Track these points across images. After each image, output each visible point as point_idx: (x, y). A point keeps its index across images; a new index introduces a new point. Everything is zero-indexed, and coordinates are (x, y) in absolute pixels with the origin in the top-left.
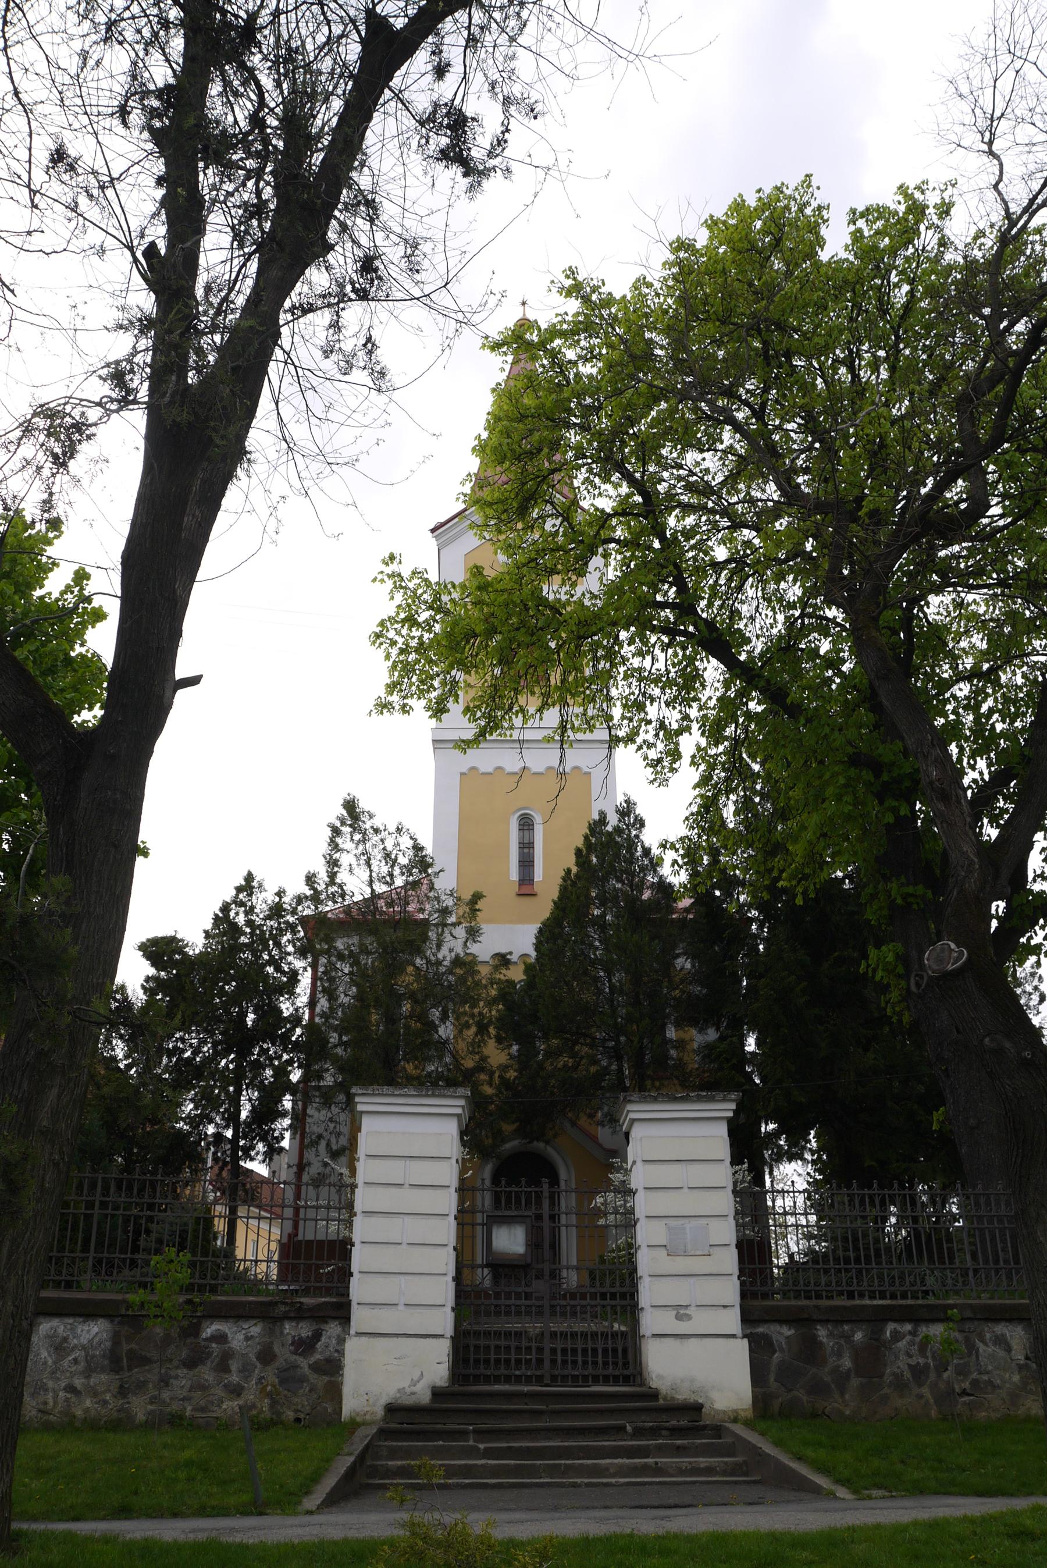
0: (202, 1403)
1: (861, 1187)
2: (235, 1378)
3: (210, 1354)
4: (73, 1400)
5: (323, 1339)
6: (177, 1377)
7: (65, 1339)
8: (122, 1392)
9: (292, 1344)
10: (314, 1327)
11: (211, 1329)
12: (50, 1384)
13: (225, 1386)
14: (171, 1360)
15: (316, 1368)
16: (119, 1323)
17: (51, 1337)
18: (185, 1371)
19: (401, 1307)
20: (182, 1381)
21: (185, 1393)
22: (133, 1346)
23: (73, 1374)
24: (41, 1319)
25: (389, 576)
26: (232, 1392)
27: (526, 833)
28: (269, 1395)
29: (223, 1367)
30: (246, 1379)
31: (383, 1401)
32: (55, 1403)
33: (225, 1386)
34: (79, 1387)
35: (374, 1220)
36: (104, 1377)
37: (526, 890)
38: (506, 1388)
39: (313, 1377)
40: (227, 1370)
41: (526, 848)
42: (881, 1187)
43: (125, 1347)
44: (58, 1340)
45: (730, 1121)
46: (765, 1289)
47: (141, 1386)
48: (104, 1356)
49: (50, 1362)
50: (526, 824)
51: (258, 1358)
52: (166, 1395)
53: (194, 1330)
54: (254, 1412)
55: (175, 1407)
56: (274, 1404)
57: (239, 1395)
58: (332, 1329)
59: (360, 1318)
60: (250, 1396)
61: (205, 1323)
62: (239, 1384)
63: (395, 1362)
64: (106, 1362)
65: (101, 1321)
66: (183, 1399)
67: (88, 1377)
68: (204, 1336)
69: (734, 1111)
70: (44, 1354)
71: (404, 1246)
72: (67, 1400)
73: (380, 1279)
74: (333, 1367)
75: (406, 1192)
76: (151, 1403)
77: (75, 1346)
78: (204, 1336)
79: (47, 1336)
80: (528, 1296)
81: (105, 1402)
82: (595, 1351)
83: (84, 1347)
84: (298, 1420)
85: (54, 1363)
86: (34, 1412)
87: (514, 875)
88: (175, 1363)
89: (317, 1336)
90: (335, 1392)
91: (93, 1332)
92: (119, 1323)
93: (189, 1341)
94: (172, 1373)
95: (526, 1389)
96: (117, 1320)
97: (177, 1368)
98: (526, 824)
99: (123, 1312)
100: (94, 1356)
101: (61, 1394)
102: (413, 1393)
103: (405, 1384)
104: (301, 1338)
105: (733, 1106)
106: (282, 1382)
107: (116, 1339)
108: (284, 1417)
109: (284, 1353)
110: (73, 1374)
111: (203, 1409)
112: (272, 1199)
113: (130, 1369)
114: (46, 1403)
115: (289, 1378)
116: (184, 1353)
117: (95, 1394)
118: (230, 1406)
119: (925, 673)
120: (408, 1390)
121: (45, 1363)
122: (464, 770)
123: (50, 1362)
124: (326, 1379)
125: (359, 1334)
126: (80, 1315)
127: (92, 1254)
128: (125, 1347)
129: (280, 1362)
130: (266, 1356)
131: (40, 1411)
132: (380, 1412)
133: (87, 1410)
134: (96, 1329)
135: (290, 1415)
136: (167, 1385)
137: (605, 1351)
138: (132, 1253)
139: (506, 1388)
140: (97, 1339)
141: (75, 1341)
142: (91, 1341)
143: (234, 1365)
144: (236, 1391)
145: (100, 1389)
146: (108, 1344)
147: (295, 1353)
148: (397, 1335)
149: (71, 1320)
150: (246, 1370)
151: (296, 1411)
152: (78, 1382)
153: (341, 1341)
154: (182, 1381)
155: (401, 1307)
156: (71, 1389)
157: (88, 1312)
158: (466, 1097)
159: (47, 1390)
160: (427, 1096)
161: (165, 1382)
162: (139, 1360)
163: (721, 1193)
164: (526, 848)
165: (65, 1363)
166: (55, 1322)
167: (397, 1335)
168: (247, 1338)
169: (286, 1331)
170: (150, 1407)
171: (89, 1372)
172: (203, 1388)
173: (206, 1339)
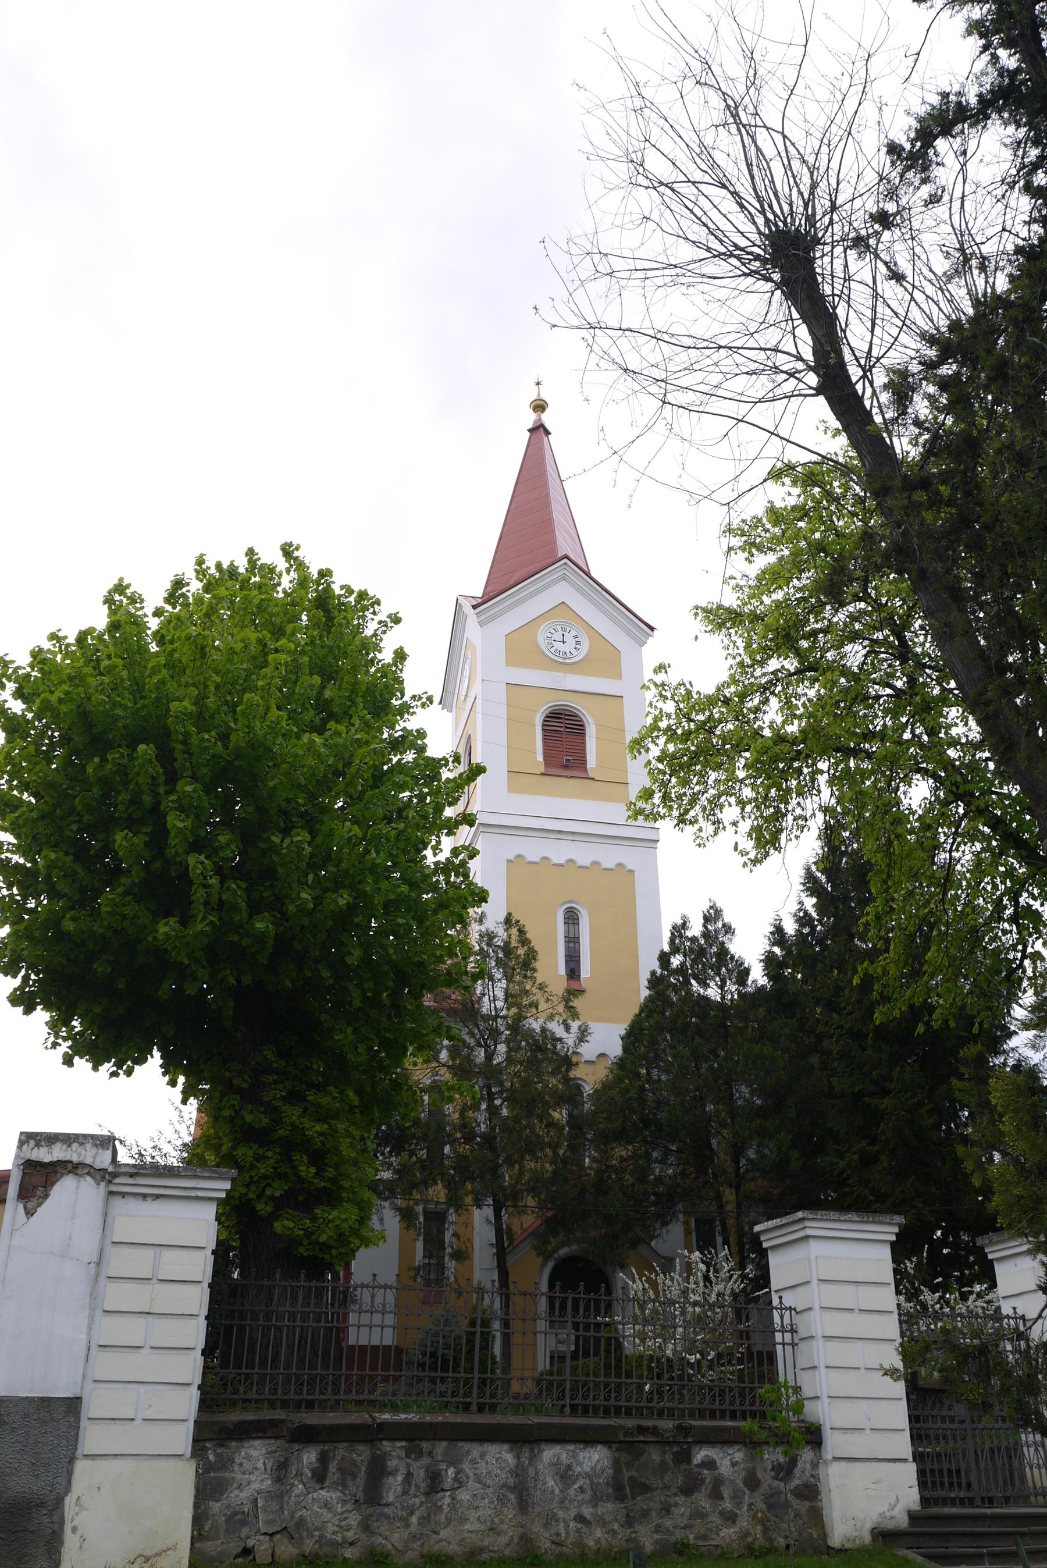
0: (703, 1531)
1: (588, 1291)
2: (727, 1505)
3: (703, 1480)
4: (584, 1529)
6: (676, 1505)
7: (569, 1467)
8: (629, 1522)
9: (773, 1469)
11: (701, 1454)
12: (561, 1514)
13: (720, 1513)
14: (669, 1488)
15: (798, 1493)
16: (617, 1450)
17: (556, 1464)
18: (683, 1498)
19: (868, 1432)
20: (682, 1508)
21: (685, 1521)
22: (633, 1473)
23: (581, 1503)
24: (543, 1446)
25: (656, 684)
26: (727, 1519)
27: (571, 927)
28: (761, 1521)
29: (716, 1495)
30: (739, 1505)
31: (868, 1526)
32: (567, 1533)
33: (720, 1513)
34: (588, 1517)
35: (834, 1345)
36: (610, 1506)
38: (954, 1510)
39: (795, 1503)
40: (719, 1497)
41: (572, 942)
42: (588, 1291)
43: (627, 1474)
44: (563, 1468)
46: (494, 1401)
47: (645, 1514)
48: (608, 1484)
49: (557, 1491)
50: (572, 918)
51: (745, 1484)
52: (668, 1523)
53: (685, 1457)
54: (750, 1540)
55: (678, 1535)
56: (766, 1531)
57: (734, 1522)
59: (834, 1443)
60: (744, 1522)
61: (695, 1449)
62: (732, 1511)
63: (873, 1486)
64: (610, 1490)
65: (599, 1447)
66: (684, 1528)
67: (595, 1506)
70: (551, 1483)
71: (862, 1371)
72: (578, 1531)
73: (847, 1404)
74: (811, 1492)
75: (857, 1317)
76: (657, 1532)
77: (579, 1474)
79: (551, 1464)
80: (952, 1420)
81: (615, 1532)
82: (941, 1471)
83: (588, 1476)
84: (788, 1547)
85: (562, 1491)
86: (548, 1544)
87: (562, 970)
88: (674, 1490)
89: (793, 1461)
90: (817, 1517)
91: (594, 1458)
92: (617, 1450)
94: (672, 1501)
95: (989, 1511)
96: (614, 1446)
97: (675, 1495)
98: (572, 918)
99: (622, 1438)
100: (598, 1484)
101: (572, 1524)
102: (892, 1518)
103: (884, 1508)
104: (779, 1464)
106: (770, 1507)
107: (616, 1464)
108: (775, 1544)
109: (766, 1478)
110: (581, 1503)
111: (704, 1538)
112: (372, 1305)
113: (634, 1497)
114: (558, 1534)
115: (775, 1504)
116: (680, 1481)
117: (604, 1524)
118: (728, 1534)
120: (888, 1515)
121: (553, 1492)
122: (511, 858)
123: (557, 1491)
124: (807, 1504)
125: (835, 1459)
126: (580, 1442)
127: (476, 1375)
128: (627, 1474)
129: (764, 1488)
130: (752, 1482)
131: (553, 1542)
132: (867, 1538)
133: (598, 1541)
134: (596, 1457)
135: (781, 1542)
136: (668, 1512)
137: (950, 1471)
138: (606, 1376)
139: (954, 1510)
140: (599, 1467)
141: (579, 1469)
142: (593, 1469)
143: (726, 1492)
144: (731, 1518)
145: (608, 1518)
146: (610, 1471)
147: (776, 1478)
148: (868, 1460)
149: (572, 1447)
150: (737, 1497)
151: (786, 1537)
152: (587, 1511)
153: (815, 1465)
154: (682, 1508)
155: (138, 1422)
156: (580, 1519)
157: (587, 1438)
158: (900, 1225)
159: (557, 1520)
160: (868, 1222)
161: (666, 1510)
162: (642, 1488)
163: (886, 1318)
164: (572, 942)
165: (572, 1492)
166: (557, 1449)
167: (868, 1460)
168: (734, 1464)
169: (766, 1456)
170: (656, 1536)
171: (595, 1501)
172: (702, 1515)
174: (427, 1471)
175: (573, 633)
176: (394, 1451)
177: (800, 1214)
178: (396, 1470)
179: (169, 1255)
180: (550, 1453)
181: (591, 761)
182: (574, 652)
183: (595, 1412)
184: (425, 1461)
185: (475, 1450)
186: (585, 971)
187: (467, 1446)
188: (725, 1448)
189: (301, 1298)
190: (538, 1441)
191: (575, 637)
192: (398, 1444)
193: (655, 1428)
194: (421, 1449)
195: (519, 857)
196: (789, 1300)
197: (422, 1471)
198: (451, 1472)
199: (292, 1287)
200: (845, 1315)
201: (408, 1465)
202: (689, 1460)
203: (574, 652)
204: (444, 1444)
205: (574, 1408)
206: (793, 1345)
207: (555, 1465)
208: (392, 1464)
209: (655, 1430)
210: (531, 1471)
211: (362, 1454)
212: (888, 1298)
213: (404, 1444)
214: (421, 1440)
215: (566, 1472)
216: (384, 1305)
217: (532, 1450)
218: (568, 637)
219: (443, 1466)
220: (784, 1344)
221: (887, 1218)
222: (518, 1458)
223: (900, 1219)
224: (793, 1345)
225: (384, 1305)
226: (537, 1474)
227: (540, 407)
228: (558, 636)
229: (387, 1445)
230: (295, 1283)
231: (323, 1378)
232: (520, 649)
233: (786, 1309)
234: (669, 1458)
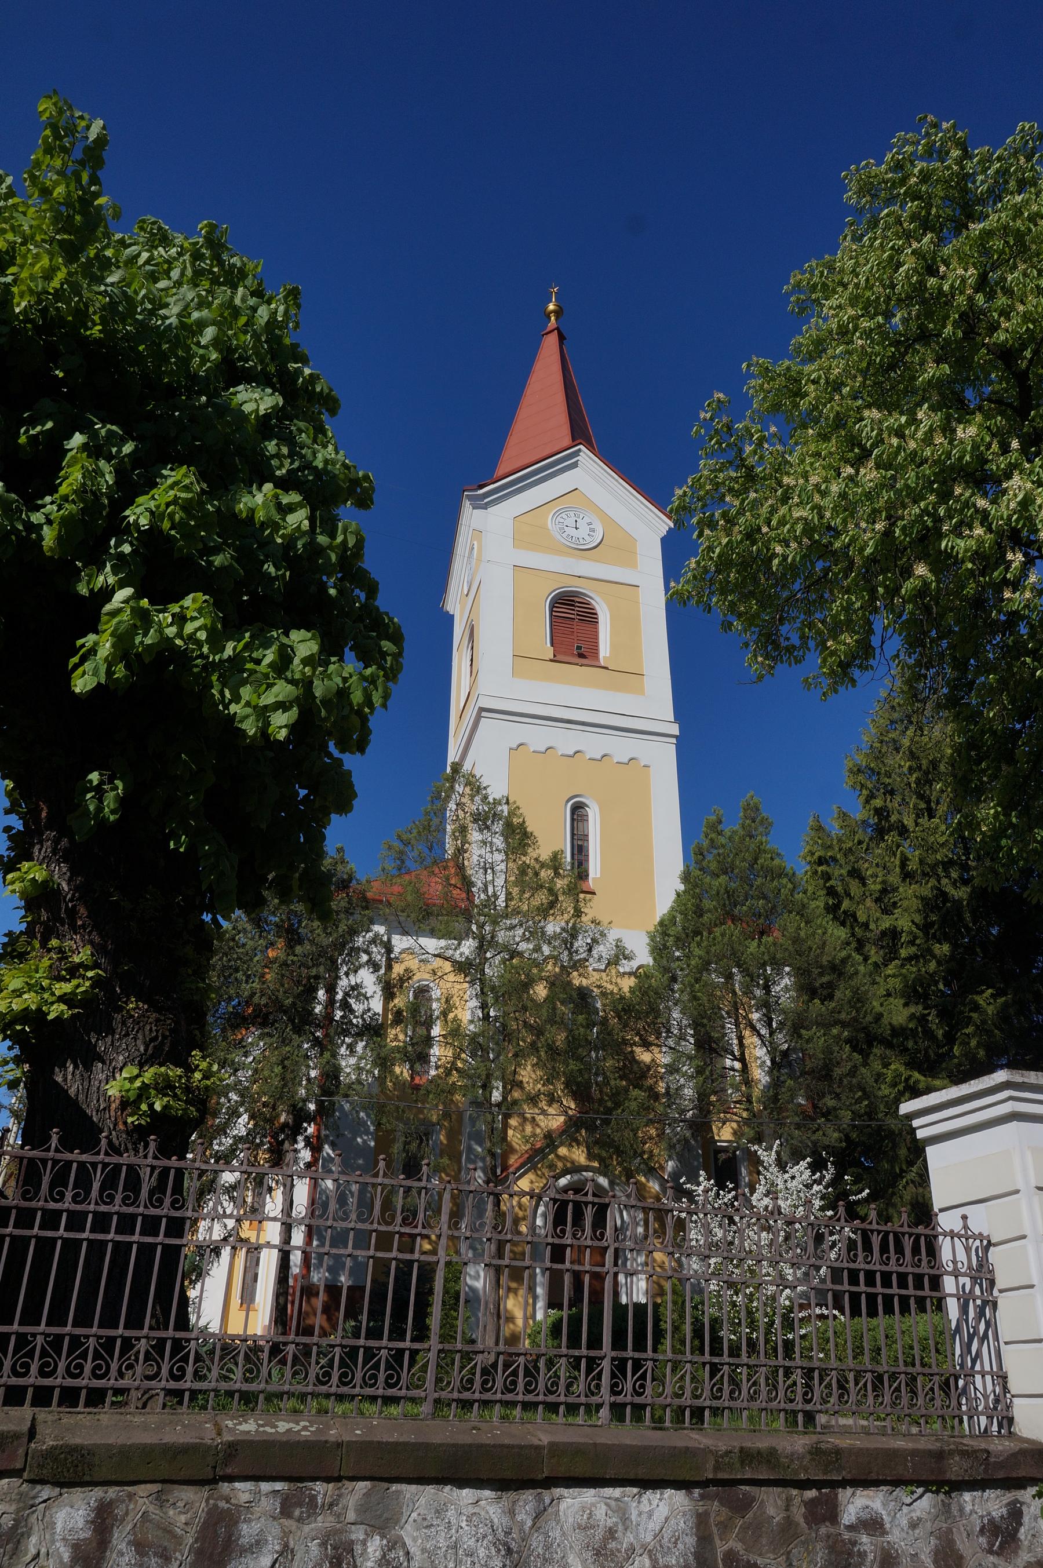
9: (982, 1531)
11: (856, 1504)
16: (702, 1497)
43: (721, 1548)
44: (599, 1534)
53: (825, 1512)
65: (669, 1492)
93: (823, 1530)
96: (697, 1492)
98: (578, 811)
107: (701, 1521)
127: (434, 1342)
140: (667, 1534)
146: (691, 1541)
166: (588, 1495)
173: (850, 1528)
174: (323, 1544)
175: (587, 520)
176: (255, 1499)
177: (1001, 1076)
178: (259, 1543)
180: (575, 1503)
181: (605, 650)
182: (587, 538)
183: (638, 1418)
184: (323, 1522)
185: (419, 1499)
187: (409, 1490)
188: (898, 1492)
189: (96, 1186)
190: (549, 1483)
191: (590, 524)
192: (265, 1487)
193: (772, 1452)
194: (313, 1498)
196: (980, 1220)
197: (314, 1546)
198: (375, 1546)
199: (82, 1165)
201: (286, 1534)
202: (832, 1515)
203: (587, 538)
204: (363, 1486)
205: (618, 1411)
208: (247, 1531)
209: (769, 1457)
210: (536, 1542)
211: (186, 1509)
213: (278, 1486)
214: (314, 1479)
215: (605, 1541)
217: (539, 1499)
219: (358, 1534)
222: (512, 1513)
226: (548, 1547)
228: (571, 522)
229: (243, 1490)
230: (84, 1157)
231: (76, 1342)
233: (975, 1237)
234: (799, 1514)
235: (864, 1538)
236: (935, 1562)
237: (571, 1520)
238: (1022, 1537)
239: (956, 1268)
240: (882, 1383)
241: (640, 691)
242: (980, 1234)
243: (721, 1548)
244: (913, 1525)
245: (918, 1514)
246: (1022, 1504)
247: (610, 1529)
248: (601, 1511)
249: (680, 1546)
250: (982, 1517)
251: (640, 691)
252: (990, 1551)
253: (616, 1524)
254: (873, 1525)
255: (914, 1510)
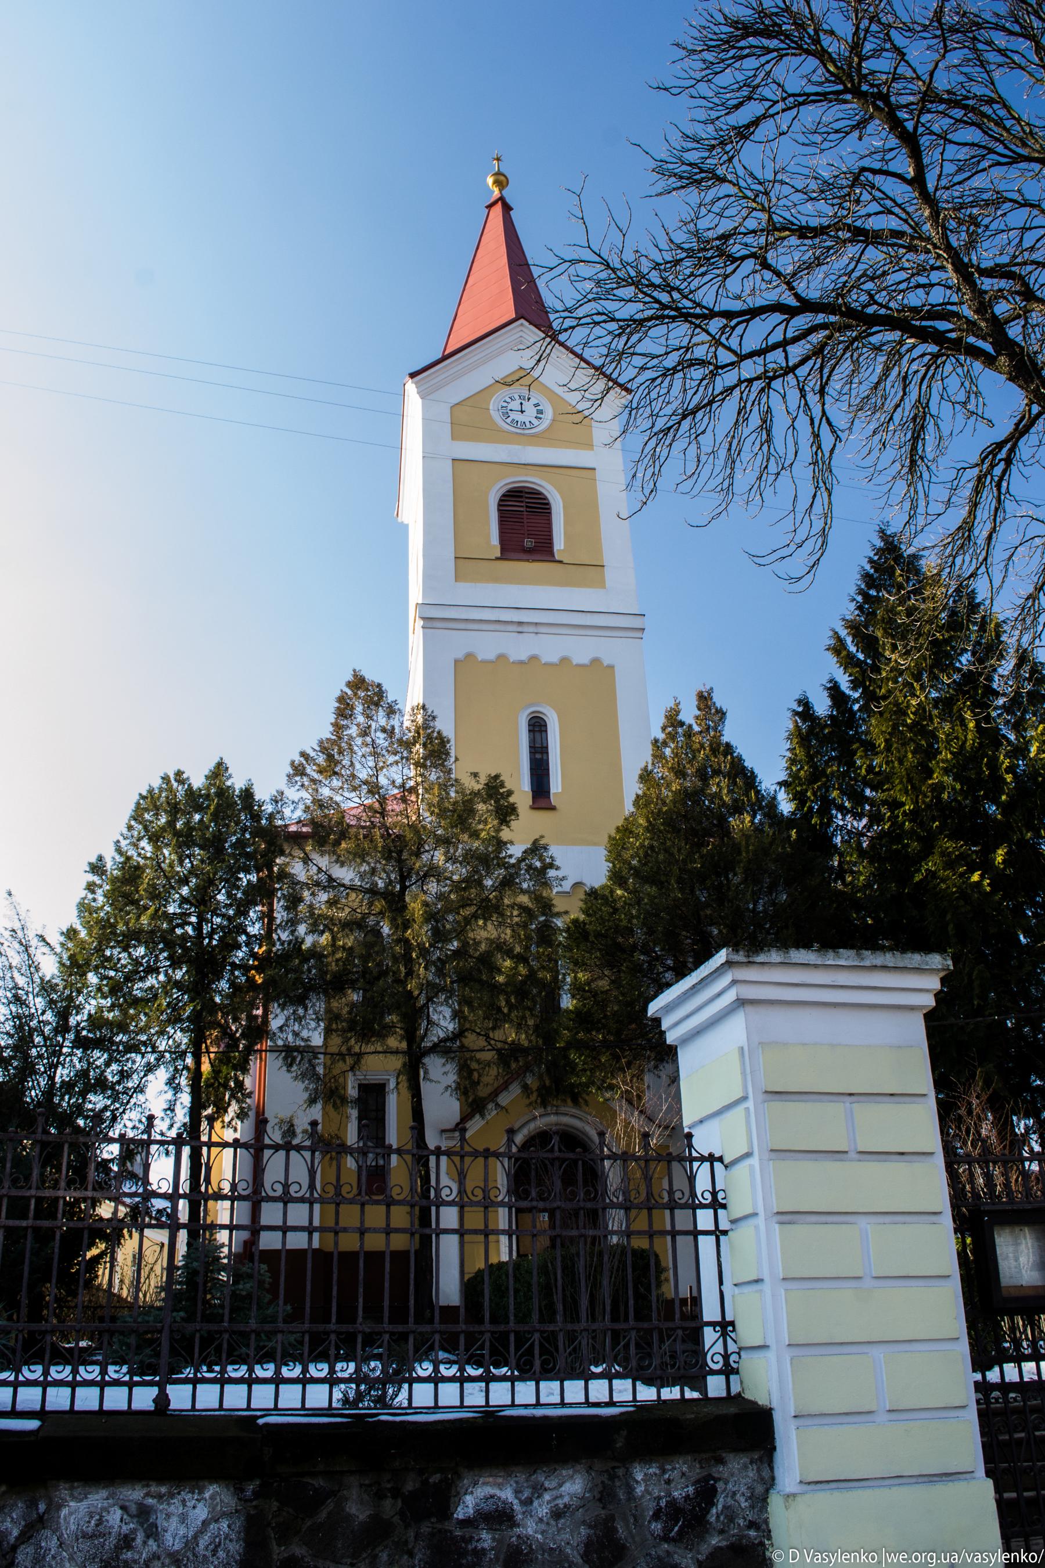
5: (721, 1501)
9: (656, 1516)
10: (697, 1472)
27: (538, 735)
37: (542, 803)
43: (278, 1552)
44: (111, 1542)
45: (930, 1017)
58: (736, 1475)
59: (794, 1454)
68: (460, 1514)
69: (938, 995)
78: (460, 1514)
89: (706, 1493)
93: (425, 1529)
98: (537, 726)
104: (672, 1503)
105: (934, 983)
119: (251, 1018)
142: (191, 1543)
146: (235, 1548)
153: (760, 1501)
163: (919, 1167)
166: (98, 1498)
173: (467, 1523)
175: (533, 401)
179: (864, 1112)
180: (81, 1510)
181: (559, 543)
182: (535, 422)
186: (556, 785)
191: (536, 405)
195: (470, 656)
200: (832, 1167)
202: (445, 1511)
203: (535, 422)
206: (718, 1233)
207: (92, 1536)
212: (920, 1125)
216: (286, 1186)
218: (528, 406)
220: (461, 1232)
221: (916, 959)
223: (936, 960)
224: (718, 1233)
225: (286, 1186)
227: (501, 181)
228: (515, 405)
232: (466, 420)
235: (485, 1535)
236: (586, 1556)
237: (73, 1527)
238: (713, 1519)
239: (672, 1199)
240: (507, 1348)
241: (601, 584)
242: (711, 1155)
243: (278, 1552)
244: (557, 1514)
245: (566, 1499)
246: (717, 1480)
247: (126, 1536)
248: (115, 1516)
249: (221, 1554)
250: (659, 1498)
251: (601, 584)
252: (665, 1538)
253: (134, 1531)
254: (499, 1517)
255: (561, 1496)
